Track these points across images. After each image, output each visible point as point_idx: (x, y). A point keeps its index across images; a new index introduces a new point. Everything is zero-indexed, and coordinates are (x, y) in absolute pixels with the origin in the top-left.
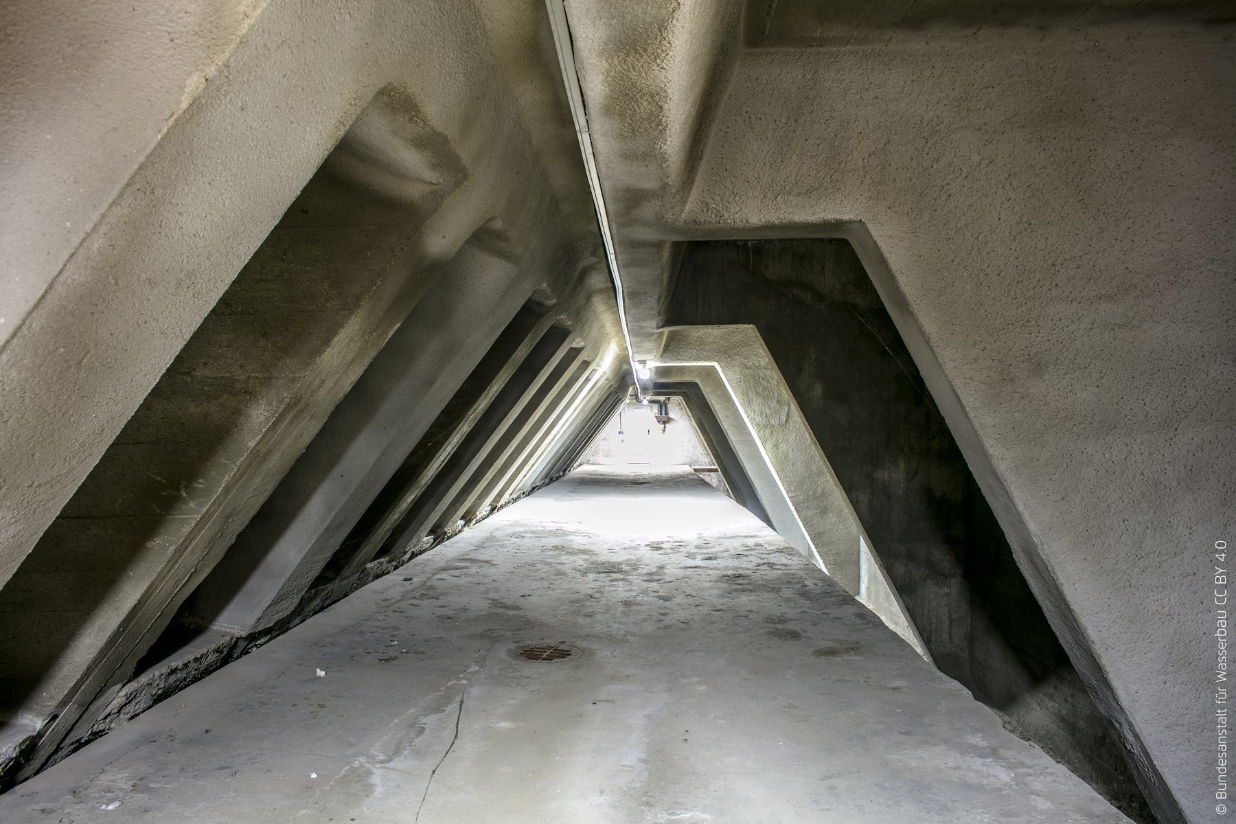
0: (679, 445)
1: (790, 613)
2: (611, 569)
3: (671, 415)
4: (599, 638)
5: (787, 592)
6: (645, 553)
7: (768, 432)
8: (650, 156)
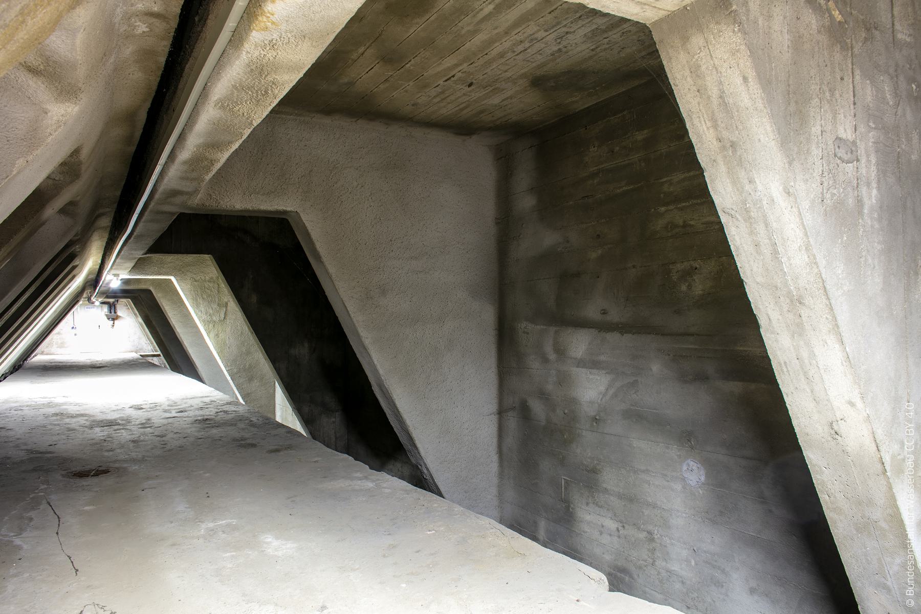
0: (129, 335)
1: (247, 435)
2: (111, 423)
3: (119, 313)
4: (125, 461)
5: (242, 425)
6: (134, 413)
7: (211, 325)
8: (199, 179)
